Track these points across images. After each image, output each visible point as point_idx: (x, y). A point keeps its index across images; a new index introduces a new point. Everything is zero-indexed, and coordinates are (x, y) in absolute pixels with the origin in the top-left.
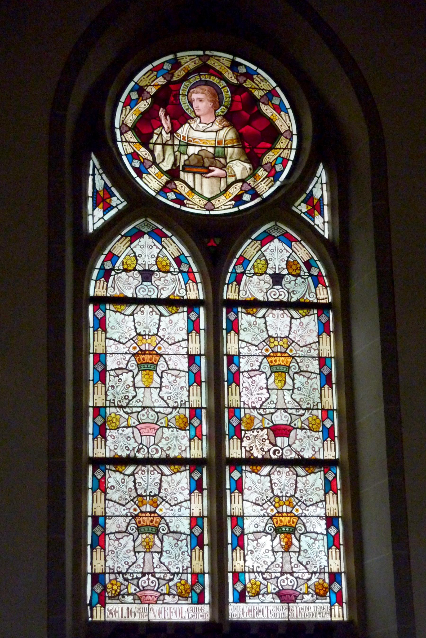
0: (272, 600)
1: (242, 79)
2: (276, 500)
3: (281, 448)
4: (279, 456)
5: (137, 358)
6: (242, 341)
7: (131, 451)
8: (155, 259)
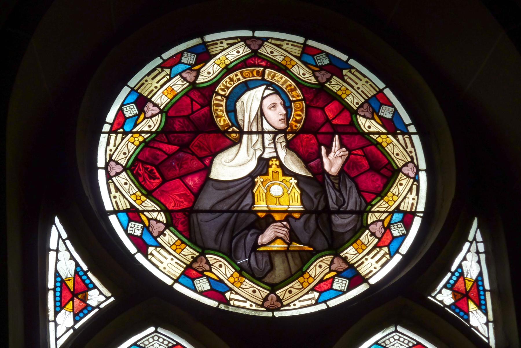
1: (323, 77)
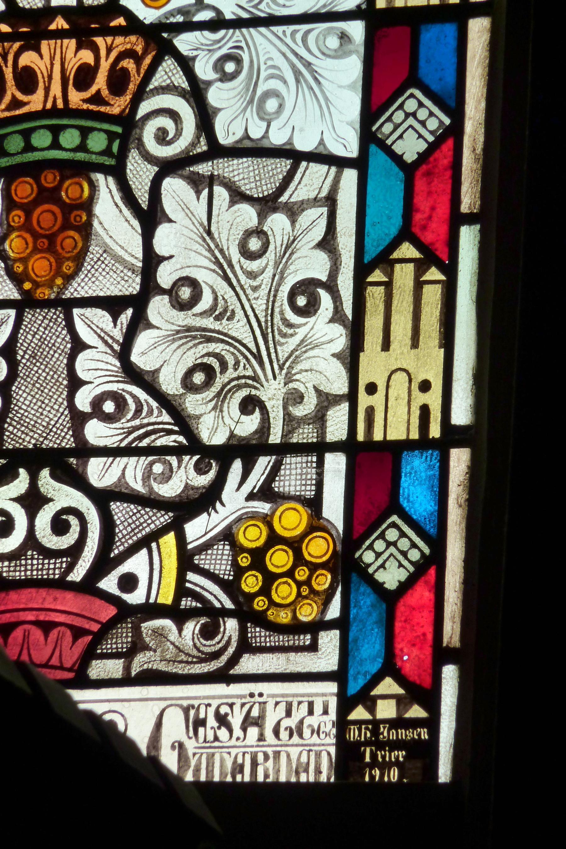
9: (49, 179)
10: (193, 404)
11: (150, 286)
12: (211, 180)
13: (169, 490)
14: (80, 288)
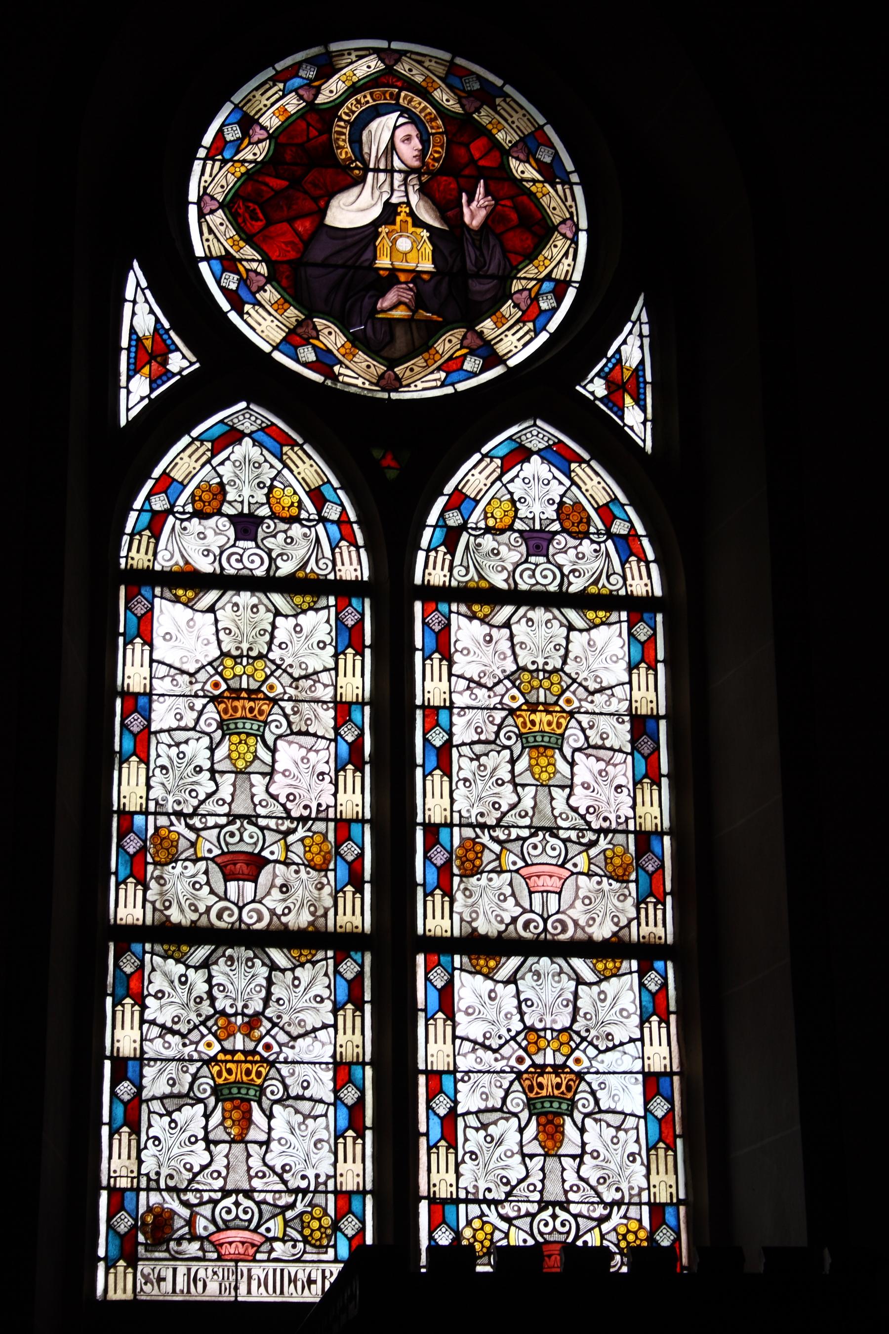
0: (200, 1254)
2: (221, 1022)
3: (541, 916)
4: (233, 924)
5: (222, 706)
6: (159, 662)
7: (201, 915)
8: (266, 490)
9: (550, 1117)
10: (601, 1188)
11: (584, 1152)
12: (600, 1120)
13: (596, 1215)
14: (562, 1151)
